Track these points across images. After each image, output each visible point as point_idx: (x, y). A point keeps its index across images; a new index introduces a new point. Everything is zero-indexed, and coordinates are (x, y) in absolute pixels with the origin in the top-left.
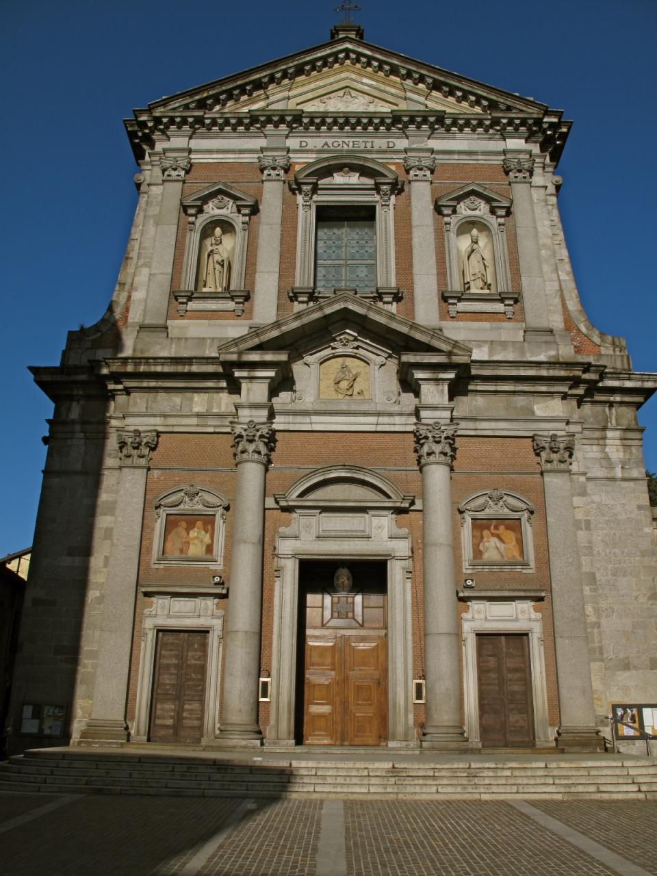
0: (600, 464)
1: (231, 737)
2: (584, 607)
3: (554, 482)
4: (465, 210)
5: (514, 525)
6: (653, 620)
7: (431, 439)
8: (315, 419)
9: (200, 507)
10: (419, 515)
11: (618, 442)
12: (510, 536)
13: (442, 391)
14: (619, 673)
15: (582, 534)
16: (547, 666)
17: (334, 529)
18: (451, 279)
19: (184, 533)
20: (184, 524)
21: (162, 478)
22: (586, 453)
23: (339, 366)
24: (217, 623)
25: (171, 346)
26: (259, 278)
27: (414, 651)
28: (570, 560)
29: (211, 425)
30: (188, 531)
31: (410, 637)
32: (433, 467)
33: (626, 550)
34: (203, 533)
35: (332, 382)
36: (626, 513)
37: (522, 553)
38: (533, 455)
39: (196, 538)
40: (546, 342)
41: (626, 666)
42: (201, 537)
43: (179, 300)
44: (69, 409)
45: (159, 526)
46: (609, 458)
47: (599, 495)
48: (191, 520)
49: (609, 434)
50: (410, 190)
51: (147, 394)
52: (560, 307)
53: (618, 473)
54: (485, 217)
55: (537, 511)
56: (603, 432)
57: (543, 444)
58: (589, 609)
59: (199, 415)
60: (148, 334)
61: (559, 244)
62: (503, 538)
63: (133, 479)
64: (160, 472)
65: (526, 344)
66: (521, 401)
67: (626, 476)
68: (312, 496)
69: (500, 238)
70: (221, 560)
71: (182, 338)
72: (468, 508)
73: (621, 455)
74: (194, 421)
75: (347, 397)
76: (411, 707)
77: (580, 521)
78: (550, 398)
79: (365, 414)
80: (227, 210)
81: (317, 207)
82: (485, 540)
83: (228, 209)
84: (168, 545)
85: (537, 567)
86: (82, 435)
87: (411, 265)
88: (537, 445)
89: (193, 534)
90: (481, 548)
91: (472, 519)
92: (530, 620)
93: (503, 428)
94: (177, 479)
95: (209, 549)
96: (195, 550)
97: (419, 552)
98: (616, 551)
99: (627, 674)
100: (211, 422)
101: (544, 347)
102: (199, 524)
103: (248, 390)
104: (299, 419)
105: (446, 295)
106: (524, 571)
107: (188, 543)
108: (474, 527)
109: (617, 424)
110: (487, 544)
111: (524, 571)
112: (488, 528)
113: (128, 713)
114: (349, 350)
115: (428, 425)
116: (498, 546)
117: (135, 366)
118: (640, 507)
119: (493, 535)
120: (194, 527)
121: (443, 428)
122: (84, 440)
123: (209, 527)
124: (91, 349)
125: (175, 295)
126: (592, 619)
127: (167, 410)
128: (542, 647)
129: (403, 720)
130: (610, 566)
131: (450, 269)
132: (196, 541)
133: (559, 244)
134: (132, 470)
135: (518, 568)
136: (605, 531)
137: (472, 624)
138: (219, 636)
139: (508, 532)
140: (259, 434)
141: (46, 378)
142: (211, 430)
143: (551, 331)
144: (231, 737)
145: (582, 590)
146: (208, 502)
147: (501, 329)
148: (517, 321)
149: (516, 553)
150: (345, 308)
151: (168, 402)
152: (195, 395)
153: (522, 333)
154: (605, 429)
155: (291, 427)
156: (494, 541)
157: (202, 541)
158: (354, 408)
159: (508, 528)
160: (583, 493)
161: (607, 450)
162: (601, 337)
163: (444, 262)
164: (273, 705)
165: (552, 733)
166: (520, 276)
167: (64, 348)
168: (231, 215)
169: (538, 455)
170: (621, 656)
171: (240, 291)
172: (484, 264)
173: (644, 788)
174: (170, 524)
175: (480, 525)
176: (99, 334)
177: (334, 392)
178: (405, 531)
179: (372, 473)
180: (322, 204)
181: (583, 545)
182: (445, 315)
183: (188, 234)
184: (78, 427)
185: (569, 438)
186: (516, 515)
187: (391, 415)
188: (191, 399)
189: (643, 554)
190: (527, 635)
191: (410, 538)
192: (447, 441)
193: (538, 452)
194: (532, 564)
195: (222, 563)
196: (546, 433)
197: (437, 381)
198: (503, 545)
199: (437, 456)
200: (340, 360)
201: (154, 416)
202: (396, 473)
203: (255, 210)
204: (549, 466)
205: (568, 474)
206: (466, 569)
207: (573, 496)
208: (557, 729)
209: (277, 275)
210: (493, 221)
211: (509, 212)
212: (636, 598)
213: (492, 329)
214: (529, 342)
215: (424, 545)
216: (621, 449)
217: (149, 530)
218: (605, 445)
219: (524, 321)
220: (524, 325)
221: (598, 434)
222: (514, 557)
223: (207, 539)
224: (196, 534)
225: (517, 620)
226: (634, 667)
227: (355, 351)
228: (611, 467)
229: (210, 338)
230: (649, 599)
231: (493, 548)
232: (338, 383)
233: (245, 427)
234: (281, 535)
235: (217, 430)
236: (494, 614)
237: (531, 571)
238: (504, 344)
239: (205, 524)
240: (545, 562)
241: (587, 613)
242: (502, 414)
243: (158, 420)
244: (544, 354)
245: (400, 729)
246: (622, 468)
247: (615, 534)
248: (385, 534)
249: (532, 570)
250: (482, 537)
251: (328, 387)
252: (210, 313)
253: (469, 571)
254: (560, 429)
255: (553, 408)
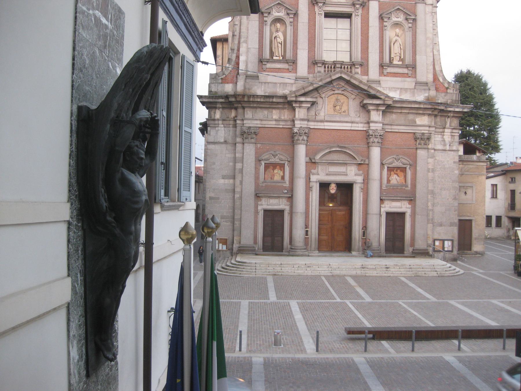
0: (441, 143)
1: (297, 251)
2: (427, 204)
3: (421, 153)
4: (394, 18)
5: (403, 170)
6: (453, 208)
7: (374, 136)
8: (326, 124)
9: (278, 160)
10: (366, 166)
11: (449, 134)
12: (401, 174)
13: (379, 114)
14: (438, 227)
15: (430, 174)
16: (411, 225)
17: (333, 171)
18: (385, 55)
19: (272, 171)
20: (272, 167)
21: (261, 147)
22: (436, 138)
23: (335, 98)
24: (287, 208)
25: (262, 86)
26: (299, 52)
27: (362, 219)
28: (424, 185)
29: (281, 125)
30: (273, 170)
31: (361, 214)
32: (374, 148)
33: (446, 180)
34: (280, 171)
35: (332, 106)
36: (448, 165)
37: (406, 182)
38: (413, 141)
39: (277, 173)
40: (424, 90)
41: (441, 225)
42: (279, 172)
43: (263, 63)
44: (215, 113)
45: (262, 168)
46: (445, 141)
47: (440, 156)
48: (274, 166)
49: (446, 130)
50: (369, 4)
51: (252, 109)
52: (432, 70)
53: (448, 148)
54: (403, 22)
55: (414, 165)
56: (444, 129)
57: (418, 136)
58: (429, 204)
59: (276, 120)
60: (251, 80)
61: (435, 35)
62: (399, 175)
63: (249, 148)
64: (260, 145)
65: (416, 90)
66: (411, 117)
67: (451, 149)
68: (324, 158)
69: (409, 34)
70: (287, 183)
71: (266, 83)
72: (386, 163)
73: (450, 139)
74: (274, 123)
75: (339, 114)
76: (361, 239)
77: (430, 169)
78: (423, 116)
79: (347, 122)
80: (281, 14)
81: (325, 13)
82: (392, 175)
83: (282, 12)
84: (266, 176)
85: (411, 187)
86: (222, 126)
87: (368, 48)
88: (416, 137)
89: (276, 171)
90: (390, 179)
91: (387, 167)
92: (407, 208)
93: (402, 129)
94: (268, 148)
95: (283, 178)
96: (277, 178)
97: (366, 181)
98: (443, 180)
99: (441, 228)
100: (281, 123)
101: (423, 91)
102: (278, 167)
103: (299, 111)
104: (319, 124)
105: (383, 65)
106: (406, 189)
107: (274, 175)
108: (388, 170)
109: (450, 126)
110: (392, 177)
111: (406, 189)
112: (393, 171)
113: (255, 242)
114: (340, 92)
115: (373, 130)
116: (397, 178)
117: (248, 98)
118: (454, 162)
119: (395, 174)
120: (276, 169)
121: (379, 131)
122: (223, 128)
123: (282, 169)
124: (222, 83)
125: (261, 61)
126: (430, 208)
127: (262, 117)
128: (410, 218)
129: (358, 244)
130: (439, 186)
131: (385, 51)
132: (277, 174)
133: (435, 35)
134: (249, 144)
135: (404, 188)
136: (439, 172)
137: (385, 209)
138: (288, 213)
139: (401, 172)
140: (304, 132)
141: (205, 100)
142: (281, 126)
143: (427, 83)
144: (297, 251)
145: (427, 197)
146: (282, 159)
147: (405, 81)
148: (413, 77)
149: (403, 181)
150: (341, 77)
151: (262, 114)
152: (273, 110)
153: (414, 84)
154: (444, 128)
155: (316, 127)
156: (395, 176)
157: (279, 174)
158: (342, 119)
159: (401, 171)
160: (433, 157)
161: (444, 137)
162: (448, 84)
163: (383, 46)
164: (310, 238)
165: (411, 249)
166: (416, 55)
167: (209, 83)
168: (284, 16)
169: (416, 141)
170: (439, 221)
171: (291, 60)
172: (400, 47)
173: (439, 273)
174: (267, 167)
175: (391, 170)
176: (224, 76)
177: (333, 110)
178: (361, 172)
179: (349, 149)
180: (327, 12)
181: (430, 178)
182: (381, 74)
183: (264, 26)
184: (220, 122)
185: (429, 134)
186: (405, 166)
187: (357, 123)
188: (272, 112)
189: (453, 182)
190: (405, 213)
191: (363, 176)
192: (380, 137)
193: (416, 139)
194: (409, 186)
195: (288, 184)
196: (419, 132)
197: (377, 110)
198: (398, 178)
199: (376, 143)
200: (336, 95)
201: (257, 120)
202: (358, 148)
203: (296, 14)
204: (420, 146)
205: (426, 150)
206: (384, 188)
207: (428, 158)
208: (413, 248)
209: (307, 51)
210: (407, 25)
211: (415, 20)
212: (448, 199)
213: (401, 81)
214: (417, 89)
215: (368, 179)
216: (450, 137)
217: (258, 170)
218: (444, 135)
219: (415, 77)
220: (415, 80)
221: (441, 130)
222: (402, 183)
223: (282, 174)
224: (277, 171)
225: (401, 208)
226: (444, 225)
227: (343, 92)
228: (445, 145)
229: (279, 83)
230: (453, 199)
231: (395, 179)
232: (335, 106)
233: (298, 129)
234: (312, 173)
235: (284, 127)
236: (330, 171)
237: (409, 189)
238: (406, 90)
239: (280, 167)
240: (414, 185)
241: (429, 205)
242: (402, 122)
243: (258, 122)
244: (423, 95)
245: (357, 247)
246: (450, 145)
247: (443, 173)
248: (353, 173)
249: (409, 188)
250: (391, 175)
251: (331, 108)
252: (278, 69)
253: (385, 188)
254: (425, 130)
255: (423, 121)
